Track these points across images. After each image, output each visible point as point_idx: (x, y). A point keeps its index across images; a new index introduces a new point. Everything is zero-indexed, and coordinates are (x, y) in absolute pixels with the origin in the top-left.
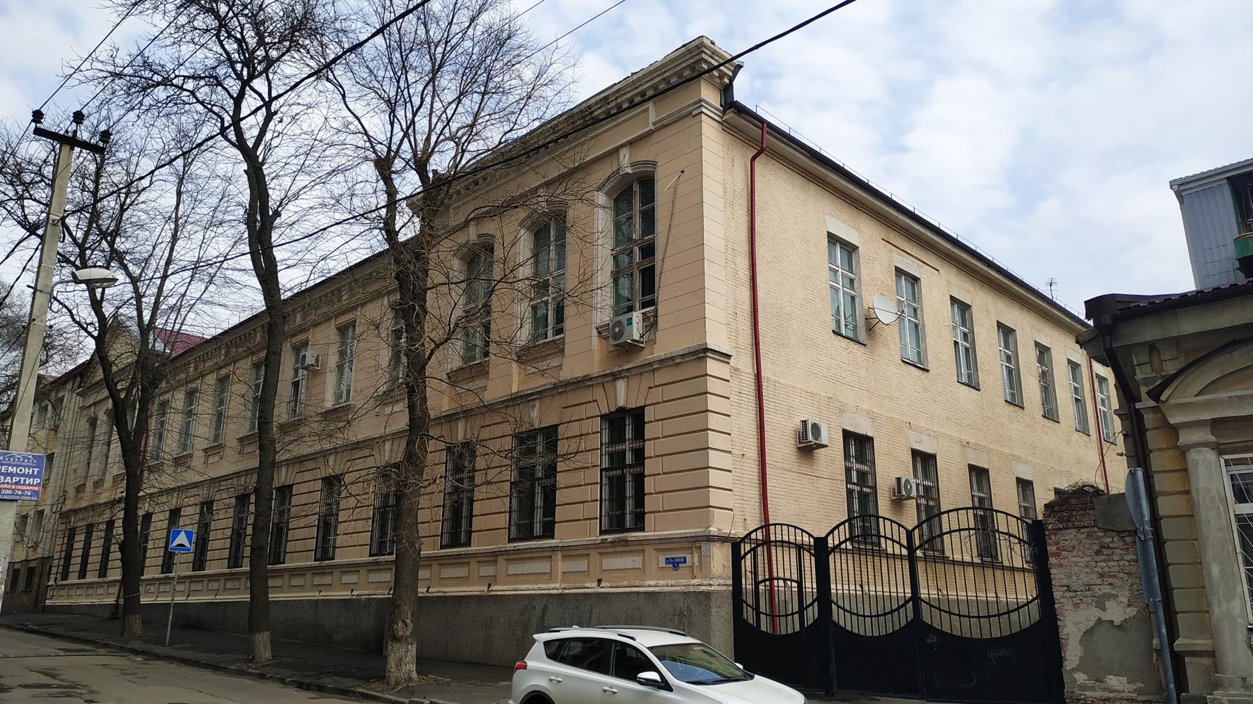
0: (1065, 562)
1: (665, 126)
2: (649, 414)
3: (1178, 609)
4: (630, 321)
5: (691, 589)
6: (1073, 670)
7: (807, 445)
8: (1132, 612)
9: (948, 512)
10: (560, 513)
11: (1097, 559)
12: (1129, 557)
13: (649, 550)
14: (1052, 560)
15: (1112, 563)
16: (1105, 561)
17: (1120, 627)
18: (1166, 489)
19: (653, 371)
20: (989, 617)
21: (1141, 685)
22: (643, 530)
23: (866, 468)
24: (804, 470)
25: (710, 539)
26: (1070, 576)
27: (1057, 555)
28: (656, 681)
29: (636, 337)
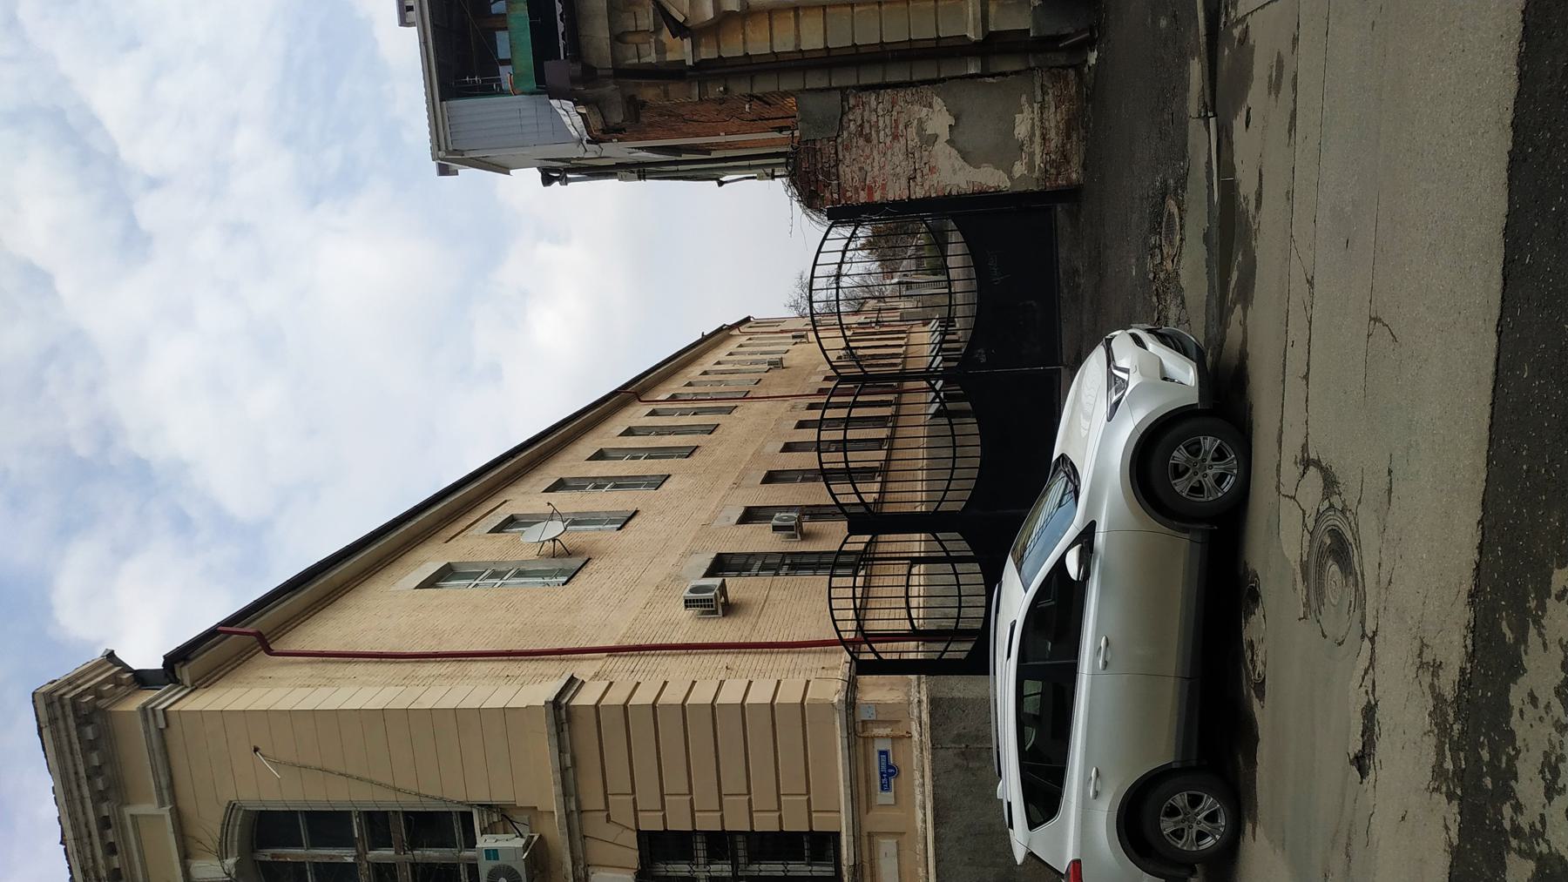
0: (880, 182)
1: (171, 785)
2: (652, 823)
3: (933, 35)
4: (492, 854)
5: (927, 737)
6: (1011, 178)
7: (717, 606)
8: (938, 102)
9: (838, 632)
10: (795, 823)
11: (875, 142)
12: (873, 103)
13: (872, 822)
14: (877, 197)
15: (881, 124)
16: (878, 132)
17: (957, 118)
18: (792, 38)
19: (581, 812)
20: (959, 585)
21: (1024, 98)
22: (838, 834)
23: (759, 563)
24: (756, 611)
25: (851, 704)
26: (896, 175)
27: (871, 190)
28: (1081, 551)
29: (519, 843)
